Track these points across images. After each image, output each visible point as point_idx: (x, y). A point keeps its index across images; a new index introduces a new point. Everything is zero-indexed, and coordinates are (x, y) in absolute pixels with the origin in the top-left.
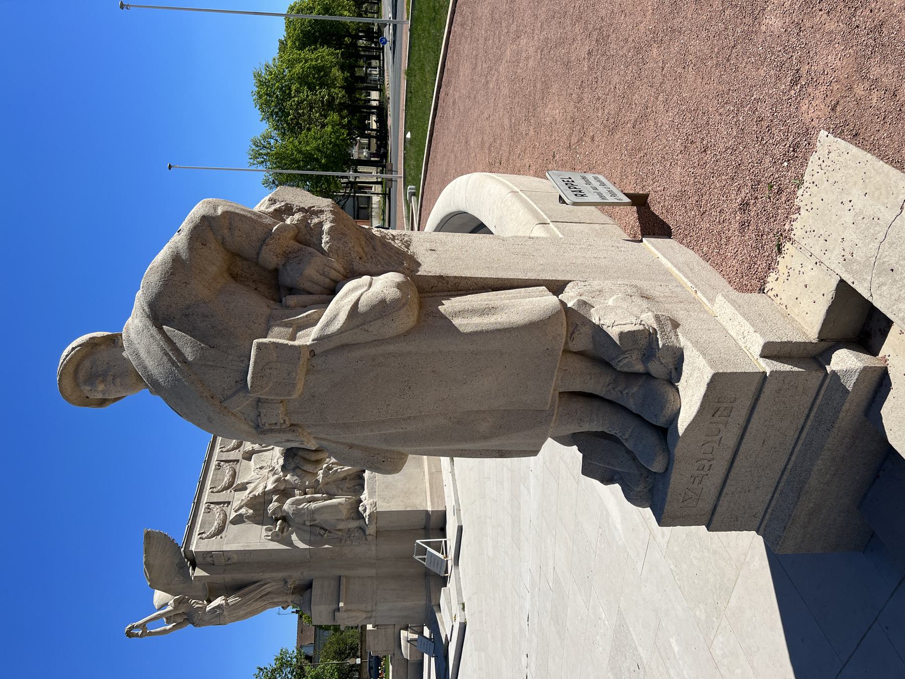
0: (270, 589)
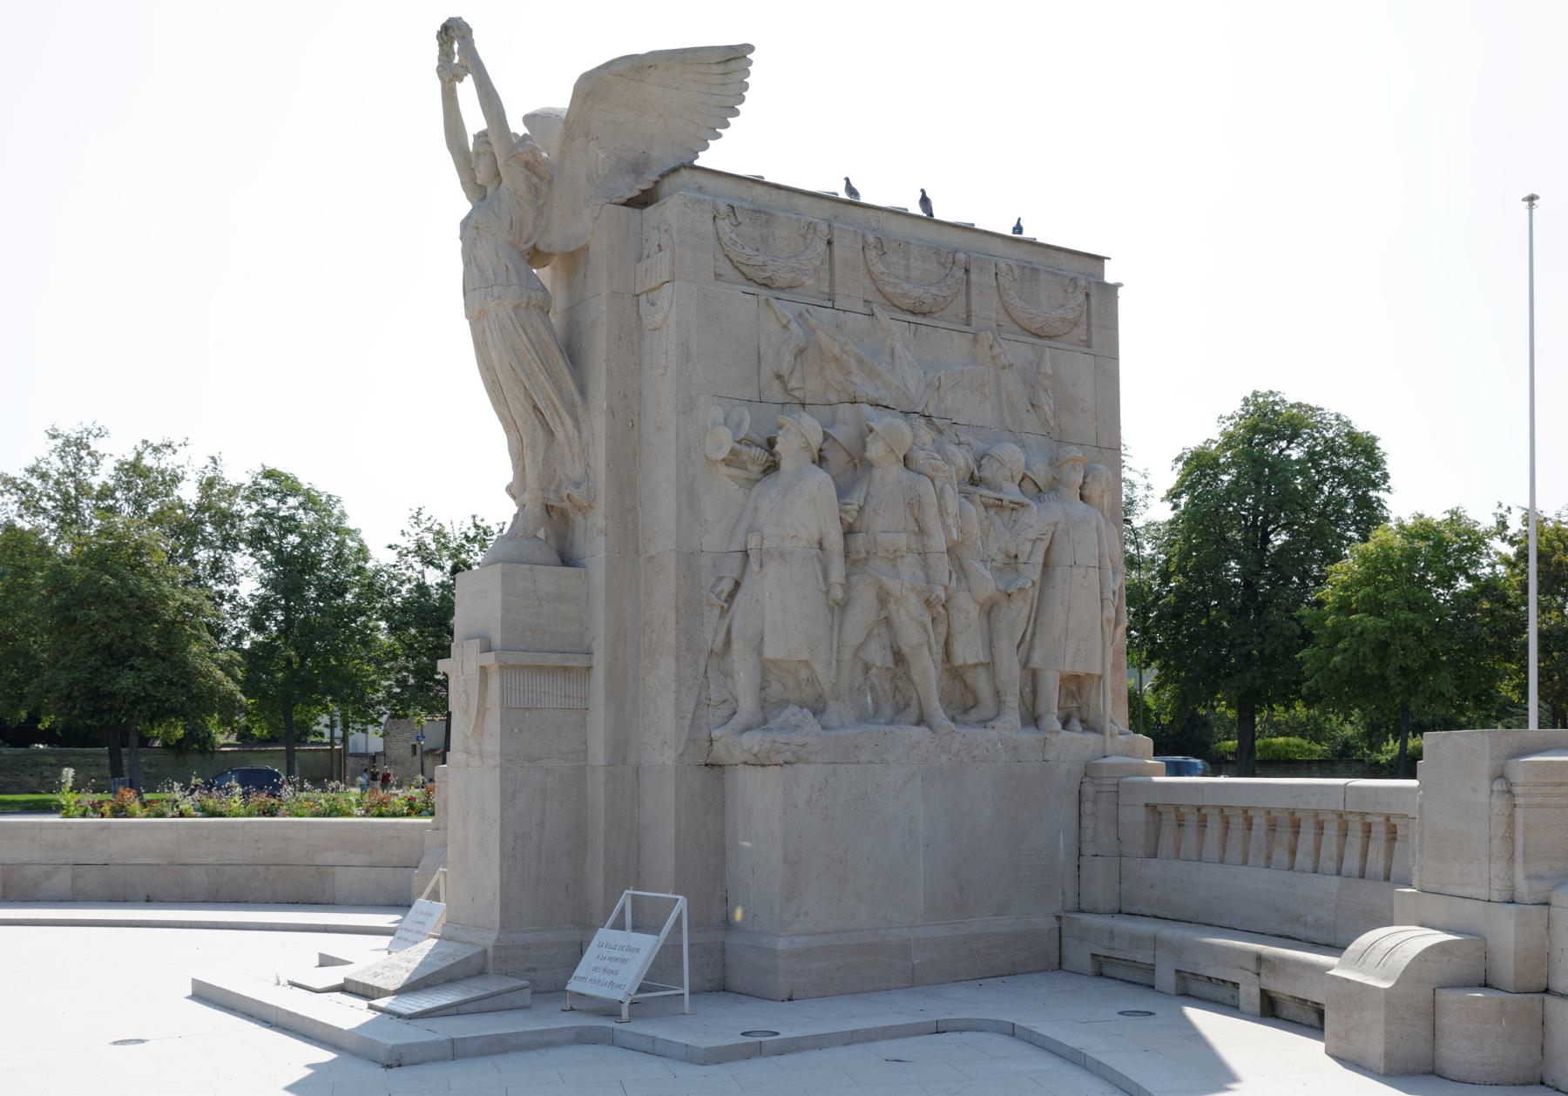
0: (560, 436)
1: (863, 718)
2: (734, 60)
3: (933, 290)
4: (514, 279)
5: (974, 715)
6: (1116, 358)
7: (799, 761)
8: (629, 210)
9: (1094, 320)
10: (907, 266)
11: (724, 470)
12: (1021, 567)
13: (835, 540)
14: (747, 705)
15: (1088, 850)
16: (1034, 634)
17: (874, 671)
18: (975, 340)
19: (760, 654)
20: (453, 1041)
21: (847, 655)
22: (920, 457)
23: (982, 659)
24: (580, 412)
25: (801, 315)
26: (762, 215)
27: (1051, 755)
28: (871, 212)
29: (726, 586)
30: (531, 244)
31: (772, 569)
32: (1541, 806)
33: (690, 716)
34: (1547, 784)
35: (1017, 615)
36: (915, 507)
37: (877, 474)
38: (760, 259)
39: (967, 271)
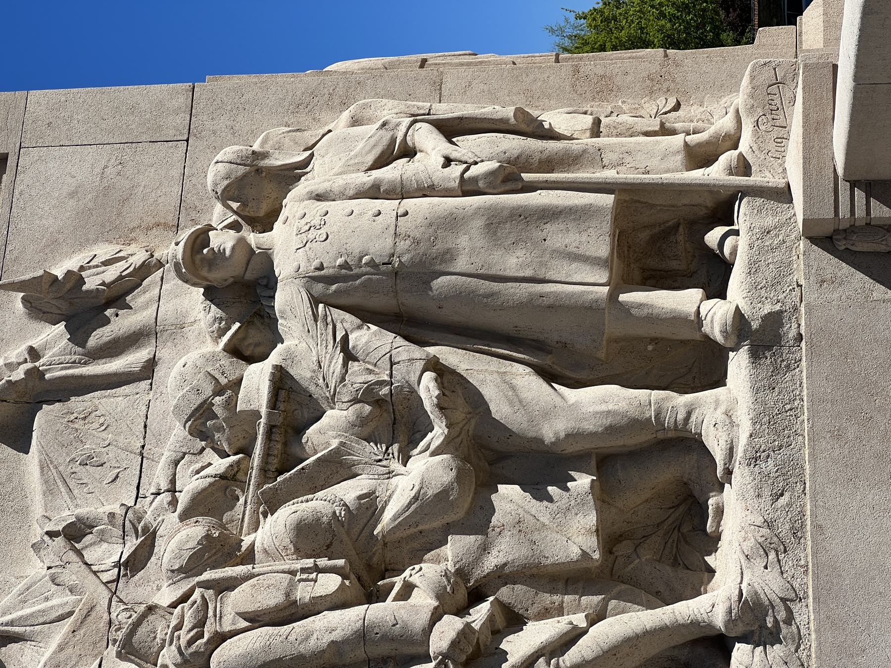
35: (512, 390)
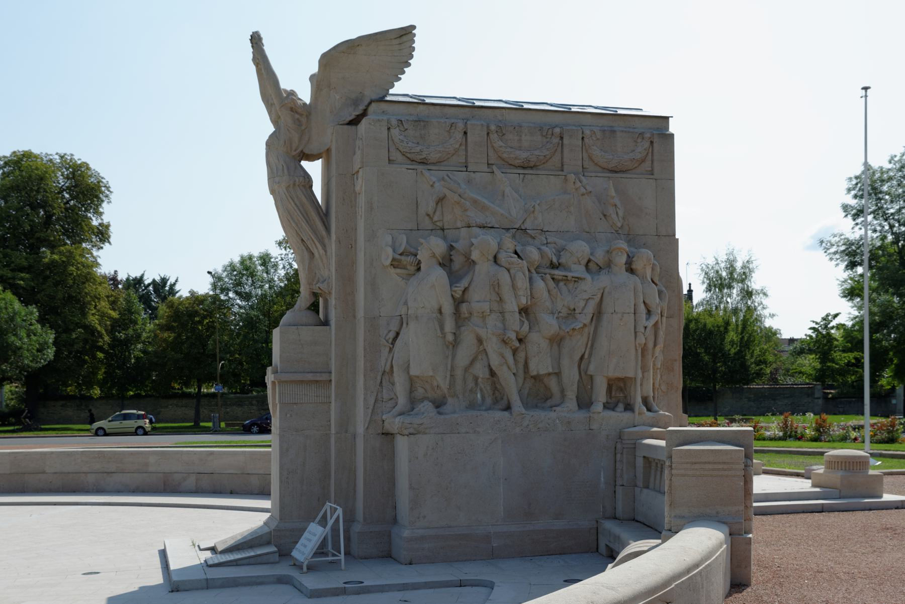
0: (316, 254)
1: (472, 406)
2: (405, 35)
3: (537, 153)
4: (286, 171)
5: (549, 403)
6: (673, 179)
7: (419, 433)
8: (349, 127)
9: (655, 158)
10: (520, 140)
11: (393, 271)
12: (578, 316)
13: (448, 308)
14: (402, 400)
15: (619, 482)
16: (590, 355)
17: (480, 380)
18: (566, 180)
19: (408, 373)
20: (207, 579)
21: (459, 373)
22: (502, 257)
23: (551, 371)
24: (326, 241)
25: (443, 179)
26: (421, 123)
27: (595, 426)
28: (498, 111)
29: (392, 335)
30: (300, 149)
31: (412, 325)
32: (683, 475)
33: (371, 407)
34: (687, 463)
35: (577, 345)
36: (496, 286)
37: (477, 267)
38: (418, 149)
39: (562, 138)
